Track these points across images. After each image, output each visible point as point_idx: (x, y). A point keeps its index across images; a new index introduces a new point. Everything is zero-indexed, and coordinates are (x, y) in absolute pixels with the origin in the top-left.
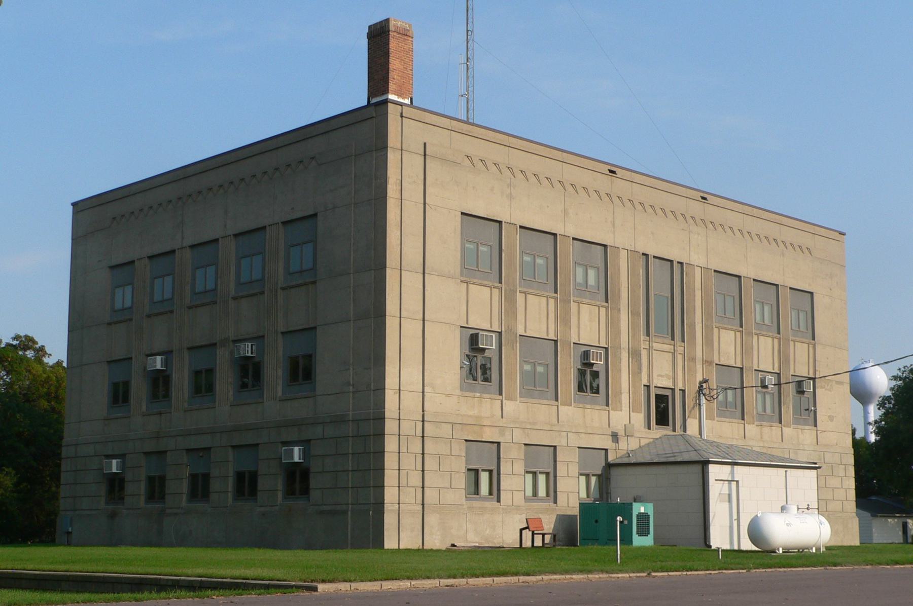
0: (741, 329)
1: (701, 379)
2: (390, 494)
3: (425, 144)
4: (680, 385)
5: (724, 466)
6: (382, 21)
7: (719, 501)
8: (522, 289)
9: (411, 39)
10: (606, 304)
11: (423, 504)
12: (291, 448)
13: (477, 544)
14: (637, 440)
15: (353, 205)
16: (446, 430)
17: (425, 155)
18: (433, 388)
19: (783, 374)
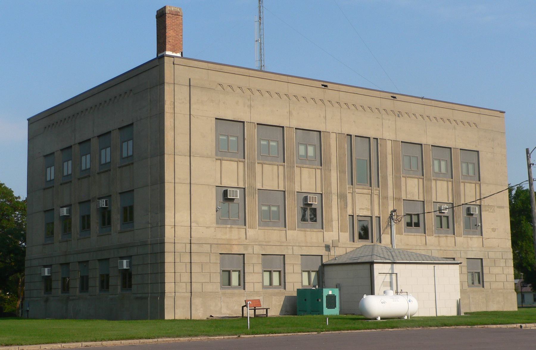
0: (423, 177)
1: (392, 209)
2: (169, 287)
4: (376, 214)
6: (162, 8)
7: (382, 286)
8: (259, 162)
9: (181, 17)
10: (321, 167)
11: (191, 292)
12: (122, 260)
13: (228, 315)
14: (344, 249)
15: (149, 118)
16: (207, 248)
17: (190, 86)
18: (197, 224)
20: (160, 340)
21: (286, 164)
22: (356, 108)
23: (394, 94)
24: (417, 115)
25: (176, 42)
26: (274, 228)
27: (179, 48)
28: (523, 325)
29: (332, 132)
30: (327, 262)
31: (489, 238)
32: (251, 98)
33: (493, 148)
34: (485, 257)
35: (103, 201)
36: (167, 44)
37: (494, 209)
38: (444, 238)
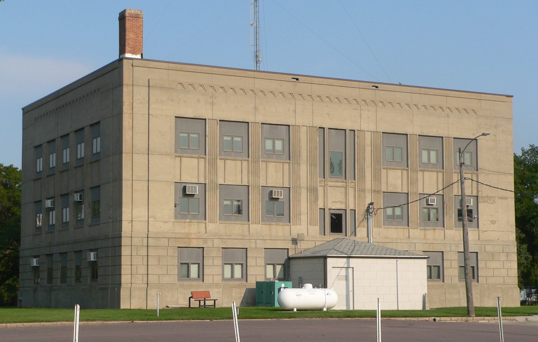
2: (125, 279)
3: (149, 80)
4: (352, 207)
5: (340, 259)
7: (337, 279)
9: (141, 19)
10: (289, 161)
11: (148, 284)
16: (165, 242)
17: (149, 86)
19: (446, 195)
20: (58, 323)
21: (250, 159)
22: (331, 100)
24: (402, 104)
25: (135, 44)
26: (236, 222)
27: (139, 50)
28: (438, 319)
29: (302, 126)
30: (293, 255)
31: (487, 231)
32: (213, 96)
33: (495, 136)
34: (481, 251)
35: (77, 195)
36: (127, 47)
37: (494, 200)
38: (432, 231)
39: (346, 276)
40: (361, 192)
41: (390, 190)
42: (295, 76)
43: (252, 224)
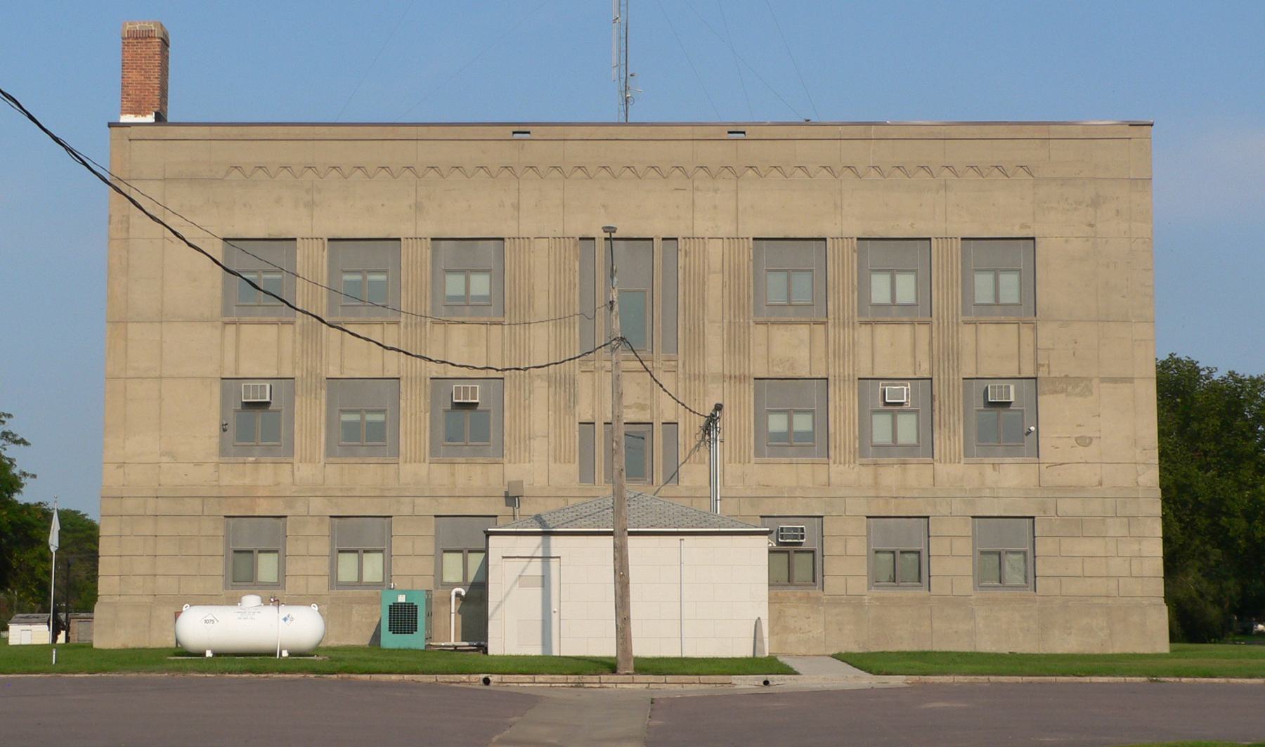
18: (173, 457)
23: (519, 126)
28: (494, 678)
33: (1091, 226)
34: (1045, 512)
38: (896, 466)
39: (543, 576)
40: (695, 380)
41: (778, 372)
42: (521, 127)
43: (835, 463)
